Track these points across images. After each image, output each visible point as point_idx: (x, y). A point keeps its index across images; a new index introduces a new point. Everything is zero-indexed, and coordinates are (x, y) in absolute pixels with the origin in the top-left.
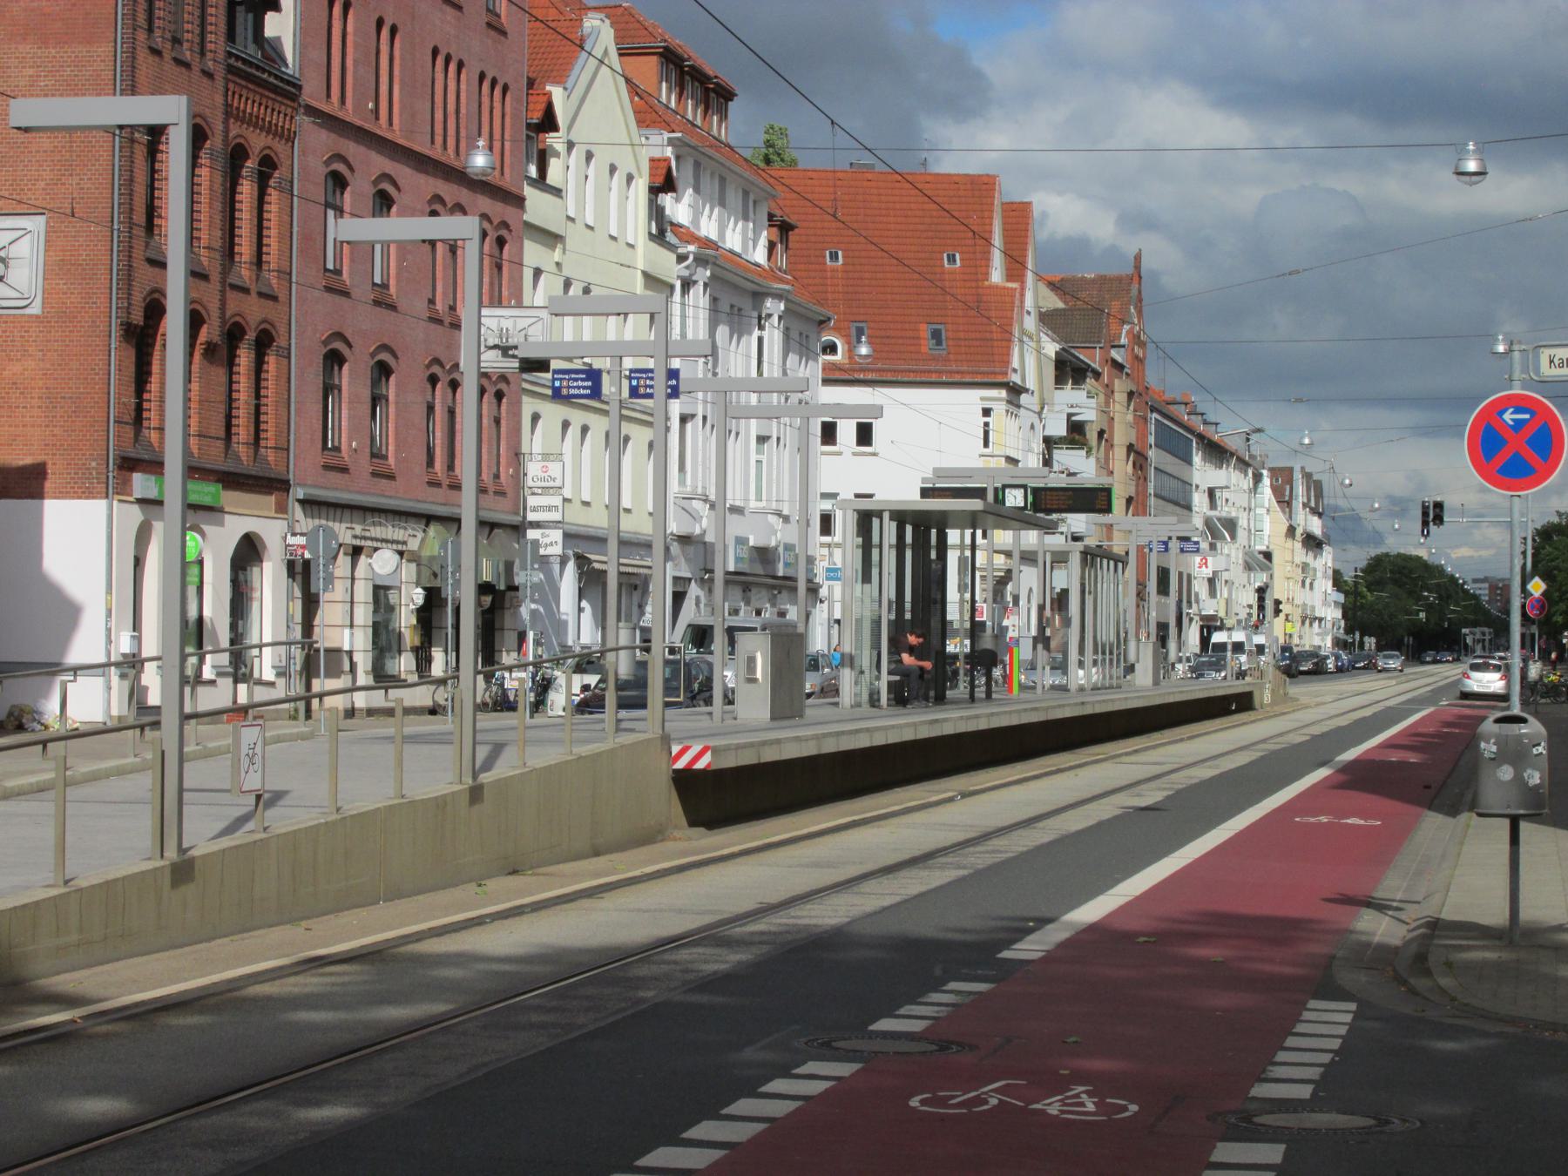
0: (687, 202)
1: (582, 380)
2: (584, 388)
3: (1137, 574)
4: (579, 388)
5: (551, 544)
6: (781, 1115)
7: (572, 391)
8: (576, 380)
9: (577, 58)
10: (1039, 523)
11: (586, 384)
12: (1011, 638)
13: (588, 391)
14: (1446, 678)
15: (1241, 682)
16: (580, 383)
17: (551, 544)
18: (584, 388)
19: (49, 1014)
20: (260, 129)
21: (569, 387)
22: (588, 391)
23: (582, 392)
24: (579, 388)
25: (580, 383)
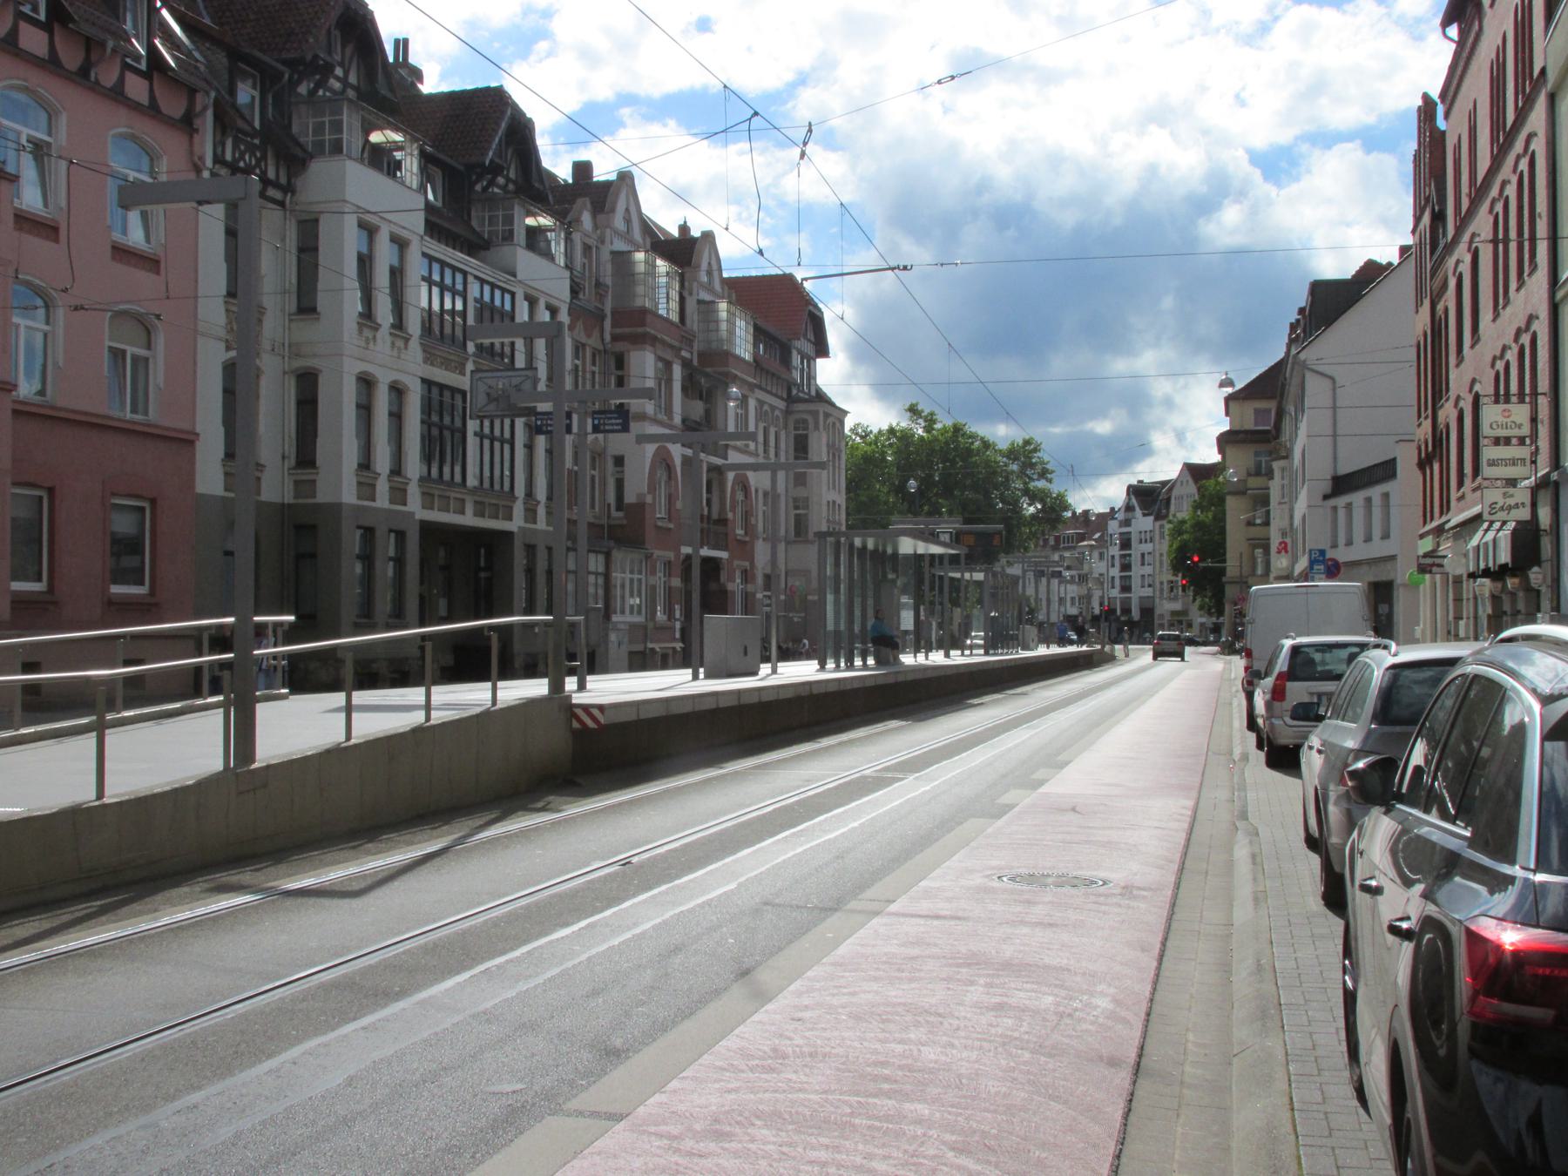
0: (1549, 606)
1: (616, 418)
2: (617, 424)
3: (228, 286)
4: (612, 425)
5: (1517, 506)
6: (1349, 277)
7: (607, 428)
8: (611, 418)
9: (439, 241)
10: (1555, 576)
11: (618, 421)
12: (548, 525)
13: (620, 427)
14: (205, 881)
15: (1349, 501)
16: (613, 421)
17: (1517, 506)
18: (617, 424)
19: (608, 799)
20: (933, 450)
21: (605, 424)
22: (620, 427)
23: (615, 427)
24: (612, 425)
25: (613, 421)
